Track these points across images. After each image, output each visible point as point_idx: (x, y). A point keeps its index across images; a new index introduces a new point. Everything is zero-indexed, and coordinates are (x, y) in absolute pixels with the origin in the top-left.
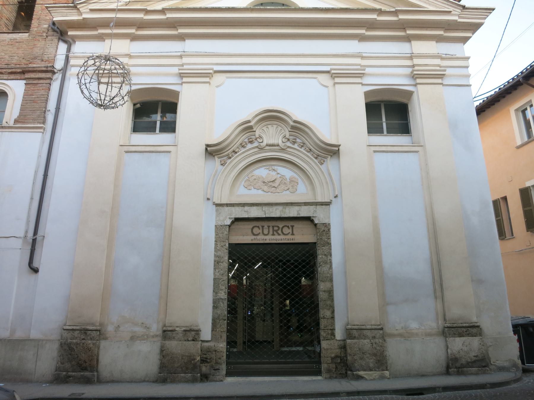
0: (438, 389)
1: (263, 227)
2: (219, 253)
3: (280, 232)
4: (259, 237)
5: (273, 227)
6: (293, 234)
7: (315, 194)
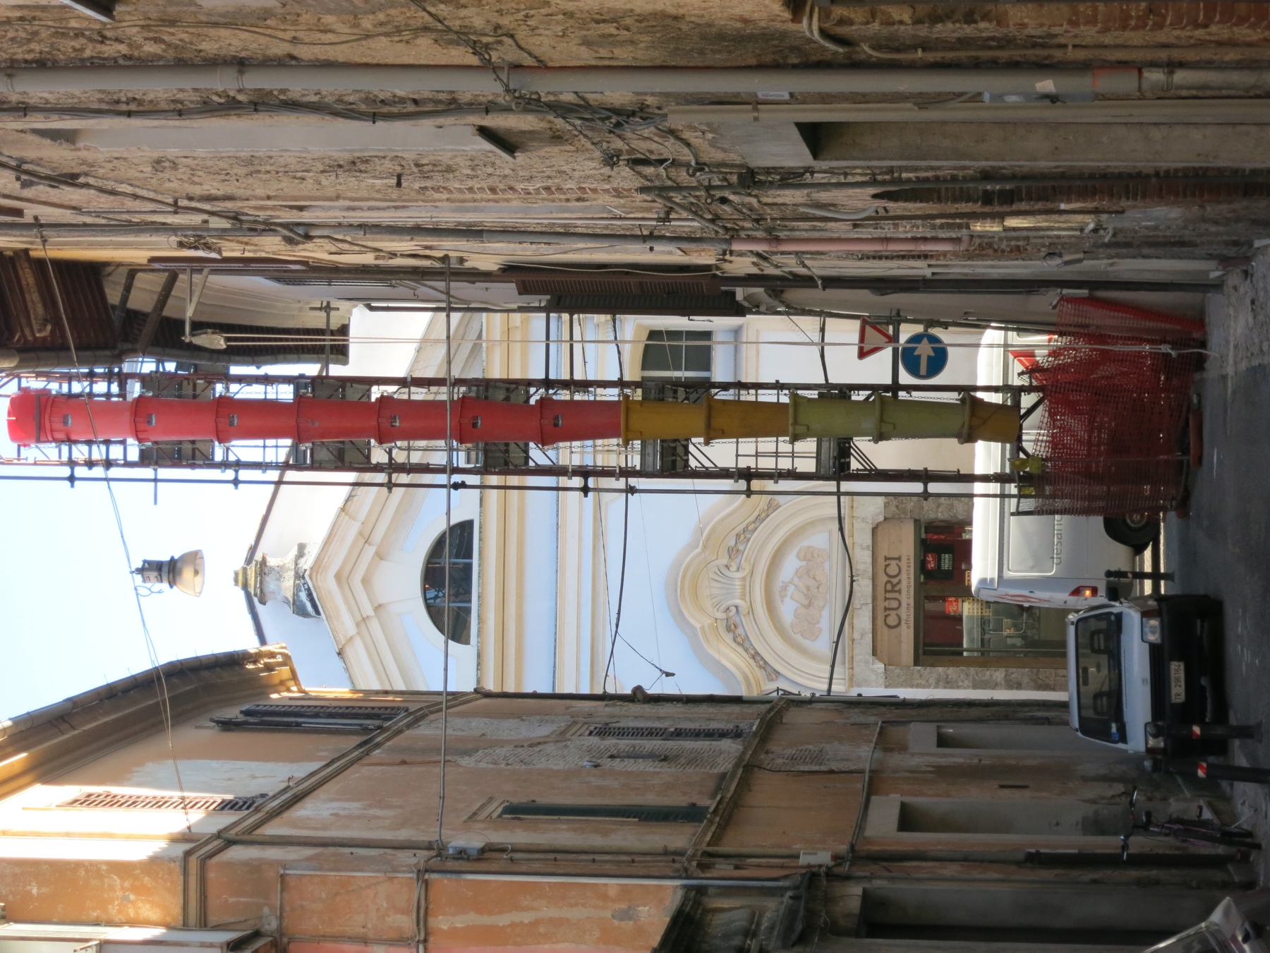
0: (291, 462)
1: (886, 609)
2: (932, 681)
3: (895, 581)
4: (904, 616)
5: (886, 591)
6: (899, 559)
7: (823, 520)
